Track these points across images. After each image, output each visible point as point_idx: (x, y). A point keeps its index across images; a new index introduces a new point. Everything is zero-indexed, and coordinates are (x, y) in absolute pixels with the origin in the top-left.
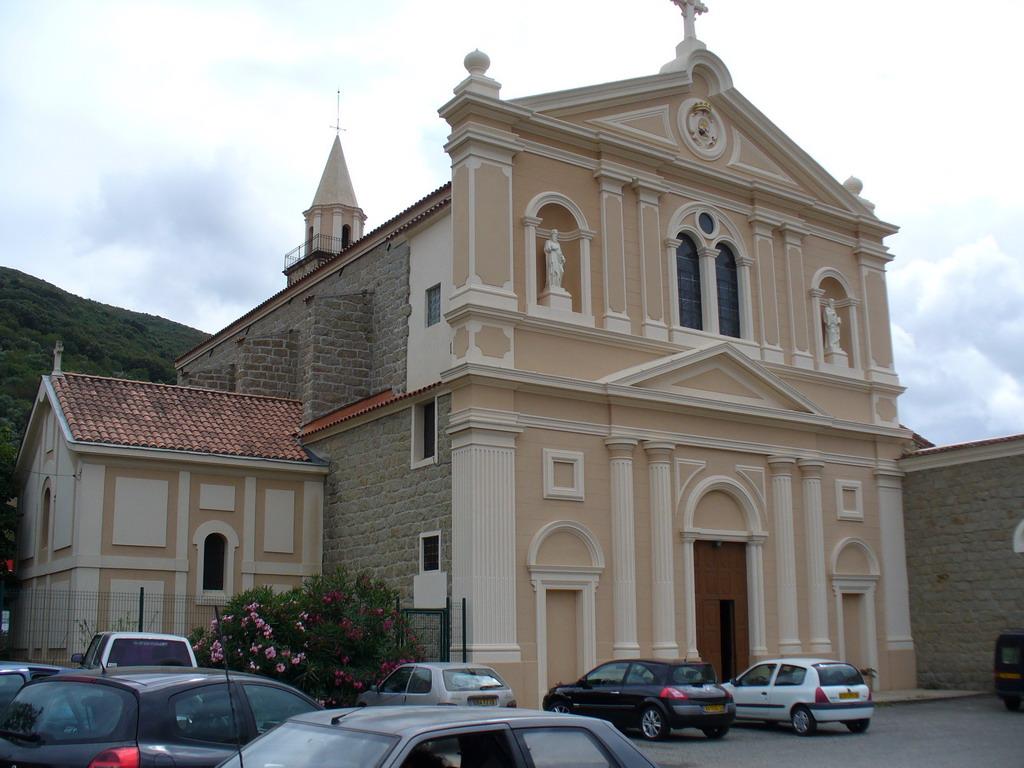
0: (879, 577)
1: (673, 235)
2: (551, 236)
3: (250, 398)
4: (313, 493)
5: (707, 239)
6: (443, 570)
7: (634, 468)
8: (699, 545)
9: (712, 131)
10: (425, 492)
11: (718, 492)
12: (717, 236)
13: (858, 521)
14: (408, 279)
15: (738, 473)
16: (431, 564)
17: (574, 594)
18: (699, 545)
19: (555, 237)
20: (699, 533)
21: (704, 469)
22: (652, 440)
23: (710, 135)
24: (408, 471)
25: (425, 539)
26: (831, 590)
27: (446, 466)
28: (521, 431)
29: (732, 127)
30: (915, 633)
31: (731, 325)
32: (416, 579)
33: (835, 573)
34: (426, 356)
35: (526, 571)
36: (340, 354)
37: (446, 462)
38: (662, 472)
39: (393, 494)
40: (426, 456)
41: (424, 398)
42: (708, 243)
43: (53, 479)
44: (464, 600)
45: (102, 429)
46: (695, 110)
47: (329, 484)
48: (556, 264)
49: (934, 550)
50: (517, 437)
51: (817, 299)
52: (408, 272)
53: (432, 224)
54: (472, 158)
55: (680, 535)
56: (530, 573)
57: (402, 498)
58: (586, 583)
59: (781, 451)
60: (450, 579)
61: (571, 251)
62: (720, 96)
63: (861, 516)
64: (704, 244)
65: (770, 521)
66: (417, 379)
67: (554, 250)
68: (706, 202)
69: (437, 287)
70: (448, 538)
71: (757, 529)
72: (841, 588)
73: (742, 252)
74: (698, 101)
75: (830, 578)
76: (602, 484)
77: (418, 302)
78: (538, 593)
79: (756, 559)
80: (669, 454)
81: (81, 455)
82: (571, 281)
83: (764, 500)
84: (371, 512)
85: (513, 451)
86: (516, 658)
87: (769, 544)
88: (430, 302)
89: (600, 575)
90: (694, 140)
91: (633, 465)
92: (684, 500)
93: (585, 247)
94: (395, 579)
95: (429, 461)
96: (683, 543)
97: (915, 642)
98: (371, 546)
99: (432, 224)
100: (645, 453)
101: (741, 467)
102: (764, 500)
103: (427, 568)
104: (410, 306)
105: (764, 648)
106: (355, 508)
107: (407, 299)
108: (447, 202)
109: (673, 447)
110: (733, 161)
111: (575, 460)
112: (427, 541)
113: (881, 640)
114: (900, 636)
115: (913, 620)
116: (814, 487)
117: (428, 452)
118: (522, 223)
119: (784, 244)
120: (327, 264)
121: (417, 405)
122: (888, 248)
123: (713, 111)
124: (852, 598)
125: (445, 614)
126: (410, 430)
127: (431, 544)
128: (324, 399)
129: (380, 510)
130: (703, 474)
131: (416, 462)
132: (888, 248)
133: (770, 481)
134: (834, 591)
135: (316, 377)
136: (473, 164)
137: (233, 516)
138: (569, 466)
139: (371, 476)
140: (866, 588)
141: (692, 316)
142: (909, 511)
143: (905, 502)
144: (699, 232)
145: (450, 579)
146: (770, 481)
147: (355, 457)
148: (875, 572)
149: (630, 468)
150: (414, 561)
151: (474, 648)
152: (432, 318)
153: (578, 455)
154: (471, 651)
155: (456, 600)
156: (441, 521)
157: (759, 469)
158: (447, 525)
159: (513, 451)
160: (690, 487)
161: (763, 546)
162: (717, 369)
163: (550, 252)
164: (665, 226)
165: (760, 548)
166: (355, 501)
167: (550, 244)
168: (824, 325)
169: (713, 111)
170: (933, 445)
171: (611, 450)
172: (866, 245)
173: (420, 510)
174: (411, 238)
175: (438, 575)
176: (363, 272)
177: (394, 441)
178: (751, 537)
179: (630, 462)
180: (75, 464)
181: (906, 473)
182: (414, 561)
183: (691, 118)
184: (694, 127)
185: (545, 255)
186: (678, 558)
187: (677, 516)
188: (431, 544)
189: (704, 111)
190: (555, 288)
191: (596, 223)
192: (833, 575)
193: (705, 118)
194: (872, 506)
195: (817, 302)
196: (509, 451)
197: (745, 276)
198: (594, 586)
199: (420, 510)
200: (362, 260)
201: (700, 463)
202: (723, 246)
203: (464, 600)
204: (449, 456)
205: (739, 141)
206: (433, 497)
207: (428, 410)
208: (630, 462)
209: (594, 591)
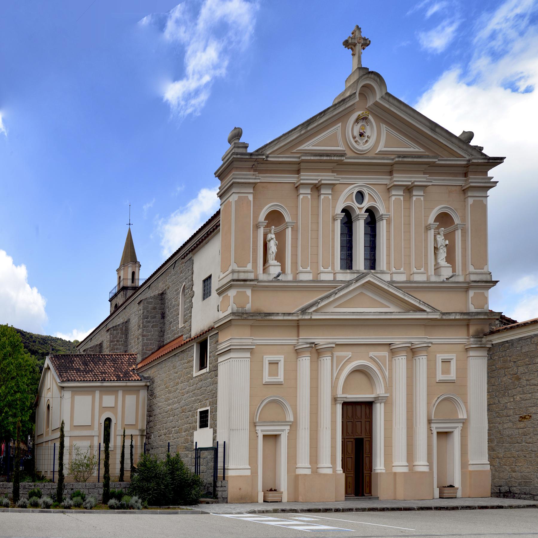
0: (292, 422)
1: (339, 210)
2: (270, 231)
3: (115, 355)
4: (143, 394)
5: (359, 208)
6: (211, 428)
7: (311, 362)
8: (346, 404)
9: (368, 133)
10: (201, 388)
11: (360, 371)
12: (366, 204)
13: (453, 382)
14: (192, 277)
15: (371, 358)
16: (204, 424)
17: (276, 437)
18: (346, 404)
19: (273, 231)
20: (346, 398)
21: (350, 358)
22: (321, 343)
23: (366, 135)
24: (192, 378)
25: (200, 412)
26: (430, 430)
27: (214, 372)
28: (254, 347)
29: (381, 124)
30: (491, 458)
31: (372, 262)
32: (195, 433)
33: (433, 418)
34: (203, 315)
35: (254, 425)
36: (152, 327)
37: (215, 369)
38: (326, 362)
39: (183, 391)
40: (200, 369)
41: (200, 339)
42: (360, 211)
43: (51, 400)
44: (225, 442)
45: (68, 376)
46: (357, 121)
47: (150, 389)
48: (273, 248)
49: (518, 398)
50: (251, 351)
51: (432, 231)
52: (193, 273)
53: (203, 246)
54: (234, 195)
55: (335, 400)
56: (255, 426)
57: (188, 392)
58: (283, 430)
59: (399, 339)
60: (215, 432)
61: (280, 237)
62: (376, 104)
63: (455, 378)
64: (358, 212)
65: (389, 387)
66: (197, 326)
67: (272, 239)
68: (359, 183)
69: (210, 277)
70: (215, 410)
71: (380, 391)
72: (262, 431)
73: (382, 210)
74: (360, 113)
75: (430, 422)
76: (292, 373)
77: (198, 288)
78: (259, 437)
79: (379, 411)
80: (330, 350)
81: (63, 388)
82: (280, 257)
83: (387, 374)
84: (171, 401)
85: (249, 359)
86: (248, 473)
87: (387, 401)
88: (204, 286)
89: (290, 425)
90: (356, 142)
91: (311, 359)
92: (337, 378)
93: (289, 232)
94: (184, 433)
95: (204, 371)
96: (336, 404)
97: (491, 465)
98: (171, 418)
99: (206, 243)
100: (317, 351)
101: (371, 354)
102: (387, 374)
103: (201, 427)
104: (194, 292)
105: (383, 467)
106: (163, 400)
107: (192, 288)
108: (218, 226)
109: (334, 346)
110: (381, 147)
111: (280, 361)
112: (201, 413)
113: (464, 464)
114: (480, 459)
115: (491, 449)
116: (422, 362)
117: (202, 365)
118: (257, 227)
119: (411, 196)
120: (138, 290)
121: (197, 343)
122: (492, 178)
123: (370, 117)
124: (444, 435)
125: (215, 450)
126: (193, 357)
127: (204, 415)
128: (146, 350)
129: (176, 399)
130: (349, 360)
131: (196, 373)
132: (492, 178)
133: (391, 361)
134: (431, 430)
135: (143, 340)
136: (233, 198)
137: (113, 409)
138: (276, 365)
139: (172, 383)
140: (456, 428)
141: (348, 262)
142: (492, 373)
143: (489, 366)
144: (355, 205)
145: (215, 432)
146: (391, 361)
147: (163, 374)
148: (462, 415)
149: (309, 361)
150: (194, 424)
151: (229, 468)
152: (206, 294)
153: (281, 358)
154: (228, 469)
155: (221, 443)
156: (210, 402)
157: (384, 353)
158: (214, 403)
159: (249, 359)
160: (341, 370)
161: (385, 403)
162: (361, 292)
163: (269, 241)
164: (334, 207)
165: (383, 404)
166: (163, 397)
167: (270, 236)
168: (436, 249)
169: (370, 117)
170: (515, 322)
171: (298, 352)
172: (474, 180)
173: (198, 397)
174: (194, 254)
175: (208, 431)
176: (160, 284)
177: (184, 364)
178: (377, 398)
179: (309, 358)
180: (61, 392)
181: (492, 344)
182: (194, 424)
183: (355, 127)
184: (356, 133)
185: (266, 244)
186: (333, 413)
187: (334, 387)
188: (204, 415)
189: (363, 119)
190: (272, 261)
191: (295, 216)
192: (431, 420)
193: (364, 123)
194: (462, 371)
195: (432, 233)
196: (247, 359)
197: (382, 227)
198: (287, 431)
199: (198, 397)
200: (163, 275)
201: (347, 353)
202: (371, 212)
203: (225, 442)
204: (216, 367)
205: (385, 131)
206: (206, 390)
207: (203, 347)
208: (309, 358)
209: (287, 435)
